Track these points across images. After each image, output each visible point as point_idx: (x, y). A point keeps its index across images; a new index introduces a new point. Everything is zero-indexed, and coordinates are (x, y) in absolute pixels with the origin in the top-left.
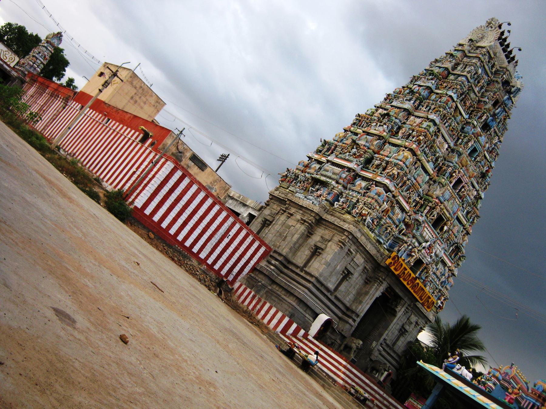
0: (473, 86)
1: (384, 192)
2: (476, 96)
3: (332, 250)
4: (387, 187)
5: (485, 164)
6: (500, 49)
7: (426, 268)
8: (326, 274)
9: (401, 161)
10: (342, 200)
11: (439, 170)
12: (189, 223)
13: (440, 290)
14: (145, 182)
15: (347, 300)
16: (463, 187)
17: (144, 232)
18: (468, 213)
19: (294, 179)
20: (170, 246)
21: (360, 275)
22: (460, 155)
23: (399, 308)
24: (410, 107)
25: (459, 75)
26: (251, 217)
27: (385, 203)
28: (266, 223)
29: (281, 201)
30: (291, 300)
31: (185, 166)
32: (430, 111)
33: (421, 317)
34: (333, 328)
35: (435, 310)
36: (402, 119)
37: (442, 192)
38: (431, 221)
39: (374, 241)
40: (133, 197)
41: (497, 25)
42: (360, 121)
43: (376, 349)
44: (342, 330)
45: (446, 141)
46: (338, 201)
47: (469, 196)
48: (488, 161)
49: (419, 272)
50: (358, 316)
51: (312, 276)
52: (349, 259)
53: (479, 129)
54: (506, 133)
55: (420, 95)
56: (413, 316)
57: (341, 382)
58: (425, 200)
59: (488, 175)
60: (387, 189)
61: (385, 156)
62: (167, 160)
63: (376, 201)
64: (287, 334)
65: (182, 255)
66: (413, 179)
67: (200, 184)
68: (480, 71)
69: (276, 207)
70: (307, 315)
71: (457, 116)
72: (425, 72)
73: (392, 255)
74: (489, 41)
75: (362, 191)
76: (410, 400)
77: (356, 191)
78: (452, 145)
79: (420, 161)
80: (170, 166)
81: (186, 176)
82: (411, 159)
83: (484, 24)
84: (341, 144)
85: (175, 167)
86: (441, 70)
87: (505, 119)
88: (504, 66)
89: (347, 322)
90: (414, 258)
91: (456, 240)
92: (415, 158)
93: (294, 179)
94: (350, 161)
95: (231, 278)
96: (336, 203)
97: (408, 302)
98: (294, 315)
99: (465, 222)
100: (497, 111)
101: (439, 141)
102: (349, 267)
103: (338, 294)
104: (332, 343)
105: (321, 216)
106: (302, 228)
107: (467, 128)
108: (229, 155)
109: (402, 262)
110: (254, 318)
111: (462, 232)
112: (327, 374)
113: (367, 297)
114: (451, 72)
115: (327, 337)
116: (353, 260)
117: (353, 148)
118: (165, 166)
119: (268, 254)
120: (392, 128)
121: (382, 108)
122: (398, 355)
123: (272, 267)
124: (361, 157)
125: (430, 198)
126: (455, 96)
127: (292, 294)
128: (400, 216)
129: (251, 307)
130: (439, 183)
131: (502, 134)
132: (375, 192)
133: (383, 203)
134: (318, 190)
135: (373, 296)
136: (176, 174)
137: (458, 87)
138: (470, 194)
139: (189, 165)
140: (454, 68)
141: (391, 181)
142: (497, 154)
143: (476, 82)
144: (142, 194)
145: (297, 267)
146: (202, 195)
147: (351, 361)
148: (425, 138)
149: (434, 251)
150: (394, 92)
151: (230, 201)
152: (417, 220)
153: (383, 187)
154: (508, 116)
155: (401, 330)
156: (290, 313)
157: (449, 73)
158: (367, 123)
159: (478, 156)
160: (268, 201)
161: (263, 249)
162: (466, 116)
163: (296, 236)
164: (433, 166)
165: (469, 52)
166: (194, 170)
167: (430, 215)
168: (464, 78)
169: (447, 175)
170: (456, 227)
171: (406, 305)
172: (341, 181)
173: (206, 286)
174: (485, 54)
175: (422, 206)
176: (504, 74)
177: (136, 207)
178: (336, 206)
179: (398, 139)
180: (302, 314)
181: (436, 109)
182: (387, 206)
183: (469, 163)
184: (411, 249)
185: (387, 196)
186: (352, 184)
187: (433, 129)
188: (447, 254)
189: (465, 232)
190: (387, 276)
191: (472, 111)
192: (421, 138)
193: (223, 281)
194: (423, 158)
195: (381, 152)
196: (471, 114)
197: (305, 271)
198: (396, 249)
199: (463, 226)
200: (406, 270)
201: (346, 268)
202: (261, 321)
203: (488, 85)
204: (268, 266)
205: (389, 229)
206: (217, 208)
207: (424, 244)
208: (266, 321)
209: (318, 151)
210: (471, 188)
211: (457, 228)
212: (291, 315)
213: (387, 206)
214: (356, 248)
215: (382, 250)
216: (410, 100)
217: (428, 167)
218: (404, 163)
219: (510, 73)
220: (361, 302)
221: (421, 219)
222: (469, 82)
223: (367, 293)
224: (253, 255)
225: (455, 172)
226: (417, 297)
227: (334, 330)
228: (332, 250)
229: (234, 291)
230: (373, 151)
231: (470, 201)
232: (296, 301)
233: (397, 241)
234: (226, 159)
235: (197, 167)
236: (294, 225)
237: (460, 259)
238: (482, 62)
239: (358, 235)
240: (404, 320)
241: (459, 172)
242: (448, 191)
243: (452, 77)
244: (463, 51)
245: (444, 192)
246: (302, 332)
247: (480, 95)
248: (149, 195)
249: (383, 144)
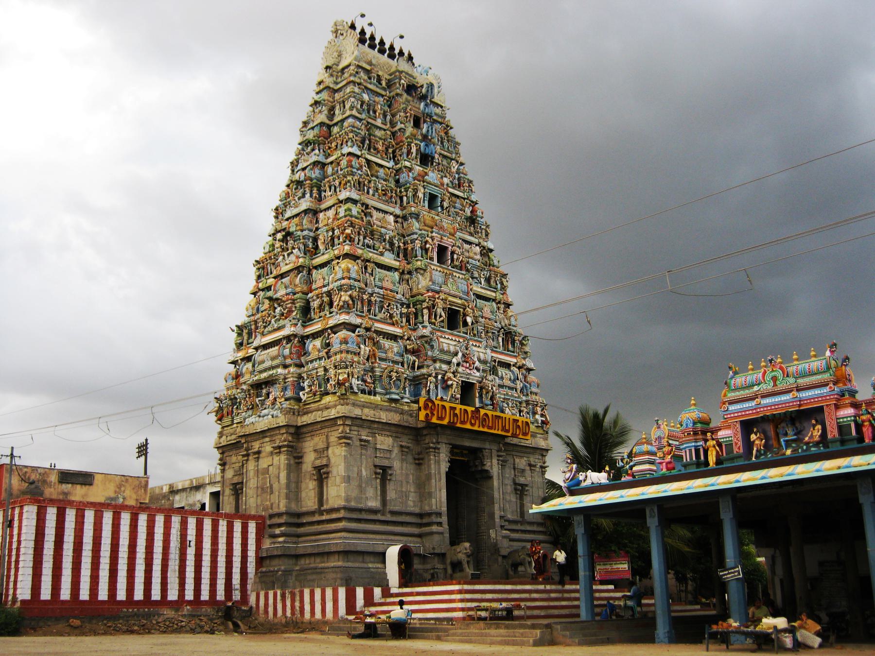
0: (370, 120)
1: (350, 333)
2: (385, 130)
3: (337, 455)
4: (350, 324)
5: (462, 205)
6: (374, 55)
7: (481, 388)
8: (354, 494)
9: (343, 278)
10: (306, 383)
11: (405, 256)
12: (120, 567)
13: (527, 402)
14: (13, 559)
15: (412, 504)
16: (453, 253)
17: (60, 626)
18: (488, 280)
19: (233, 405)
20: (115, 617)
21: (402, 460)
22: (417, 216)
23: (489, 464)
24: (308, 204)
25: (343, 121)
26: (215, 495)
27: (362, 346)
28: (238, 489)
29: (235, 446)
30: (335, 562)
31: (61, 497)
32: (338, 190)
33: (530, 453)
34: (419, 555)
35: (541, 431)
36: (310, 227)
37: (428, 279)
38: (442, 324)
39: (386, 404)
40: (11, 592)
41: (346, 27)
42: (263, 268)
43: (499, 538)
44: (434, 548)
45: (386, 212)
46: (303, 389)
47: (472, 258)
48: (464, 199)
49: (477, 400)
50: (439, 514)
51: (337, 510)
52: (370, 451)
53: (418, 168)
54: (461, 149)
55: (311, 179)
56: (517, 460)
57: (460, 614)
58: (415, 305)
59: (477, 216)
60: (351, 328)
61: (321, 287)
62: (22, 507)
63: (348, 352)
64: (358, 610)
65: (143, 617)
66: (377, 290)
67: (92, 505)
68: (366, 97)
69: (235, 459)
70: (370, 565)
71: (377, 172)
72: (300, 147)
73: (421, 403)
74: (352, 52)
75: (323, 353)
76: (598, 567)
77: (316, 360)
78: (398, 211)
79: (368, 261)
80: (30, 512)
81: (65, 509)
82: (354, 267)
83: (331, 36)
84: (259, 316)
85: (39, 508)
86: (316, 130)
87: (446, 133)
88: (393, 70)
89: (432, 533)
90: (454, 386)
91: (498, 325)
92: (359, 261)
93: (233, 405)
94: (283, 327)
95: (237, 596)
97: (494, 447)
98: (351, 579)
99: (494, 294)
100: (424, 131)
101: (377, 219)
102: (378, 462)
103: (390, 507)
104: (433, 575)
105: (295, 424)
106: (282, 460)
107: (403, 177)
108: (146, 440)
109: (441, 403)
110: (302, 623)
111: (498, 308)
112: (436, 619)
113: (433, 481)
114: (331, 123)
115: (421, 572)
116: (376, 449)
117: (275, 308)
118: (25, 516)
119: (264, 528)
120: (305, 245)
121: (280, 231)
122: (539, 524)
123: (281, 539)
124: (293, 311)
125: (420, 298)
126: (355, 150)
127: (329, 554)
128: (396, 350)
129: (289, 614)
130: (416, 270)
131: (457, 154)
132: (338, 341)
133: (359, 348)
134: (268, 395)
135: (439, 473)
136: (48, 517)
137: (351, 135)
138: (471, 255)
139: (66, 491)
140: (331, 115)
141: (348, 313)
142: (470, 182)
143: (371, 112)
144: (20, 578)
145: (312, 513)
146: (108, 518)
147: (472, 578)
148: (354, 227)
149: (476, 359)
150: (281, 200)
151: (177, 497)
152: (423, 337)
153: (345, 328)
154: (448, 126)
155: (516, 489)
156: (342, 579)
157: (329, 127)
158: (274, 264)
159: (442, 201)
160: (221, 459)
161: (252, 527)
162: (391, 164)
163: (283, 475)
164: (392, 256)
165: (336, 83)
166: (78, 493)
167: (435, 318)
168: (350, 120)
169: (419, 253)
170: (485, 309)
171: (494, 453)
172: (288, 361)
173: (207, 632)
174: (357, 73)
175: (416, 315)
176: (400, 79)
177: (23, 602)
178: (304, 398)
179: (323, 254)
180: (361, 569)
181: (343, 182)
182: (367, 349)
183: (437, 218)
184: (443, 378)
185: (358, 336)
186: (305, 354)
187: (355, 210)
188: (501, 349)
189: (502, 306)
191: (394, 152)
192: (348, 231)
193: (229, 607)
194: (371, 254)
195: (314, 287)
196: (394, 157)
197: (324, 510)
198: (423, 392)
199: (494, 300)
200: (455, 408)
201: (375, 466)
202: (313, 620)
203: (389, 106)
204: (274, 543)
205: (394, 374)
206: (160, 520)
207: (455, 360)
208: (318, 615)
209: (240, 346)
210: (466, 246)
211: (488, 308)
212: (346, 580)
213: (367, 349)
214: (368, 430)
215: (406, 408)
216: (304, 196)
217: (387, 260)
218: (350, 278)
219: (407, 73)
220: (430, 494)
221: (426, 332)
222: (360, 120)
223: (429, 477)
224: (244, 544)
225: (426, 242)
226: (500, 432)
227: (423, 558)
228: (337, 455)
229: (254, 610)
230: (304, 293)
231: (478, 264)
232: (341, 557)
233: (417, 383)
234: (147, 448)
235: (78, 487)
236: (270, 463)
237: (522, 344)
238: (359, 84)
239: (357, 412)
240: (509, 473)
241: (433, 238)
242: (436, 272)
243: (336, 130)
244: (328, 88)
245: (431, 277)
246: (377, 591)
247: (388, 125)
248: (30, 571)
249: (309, 274)
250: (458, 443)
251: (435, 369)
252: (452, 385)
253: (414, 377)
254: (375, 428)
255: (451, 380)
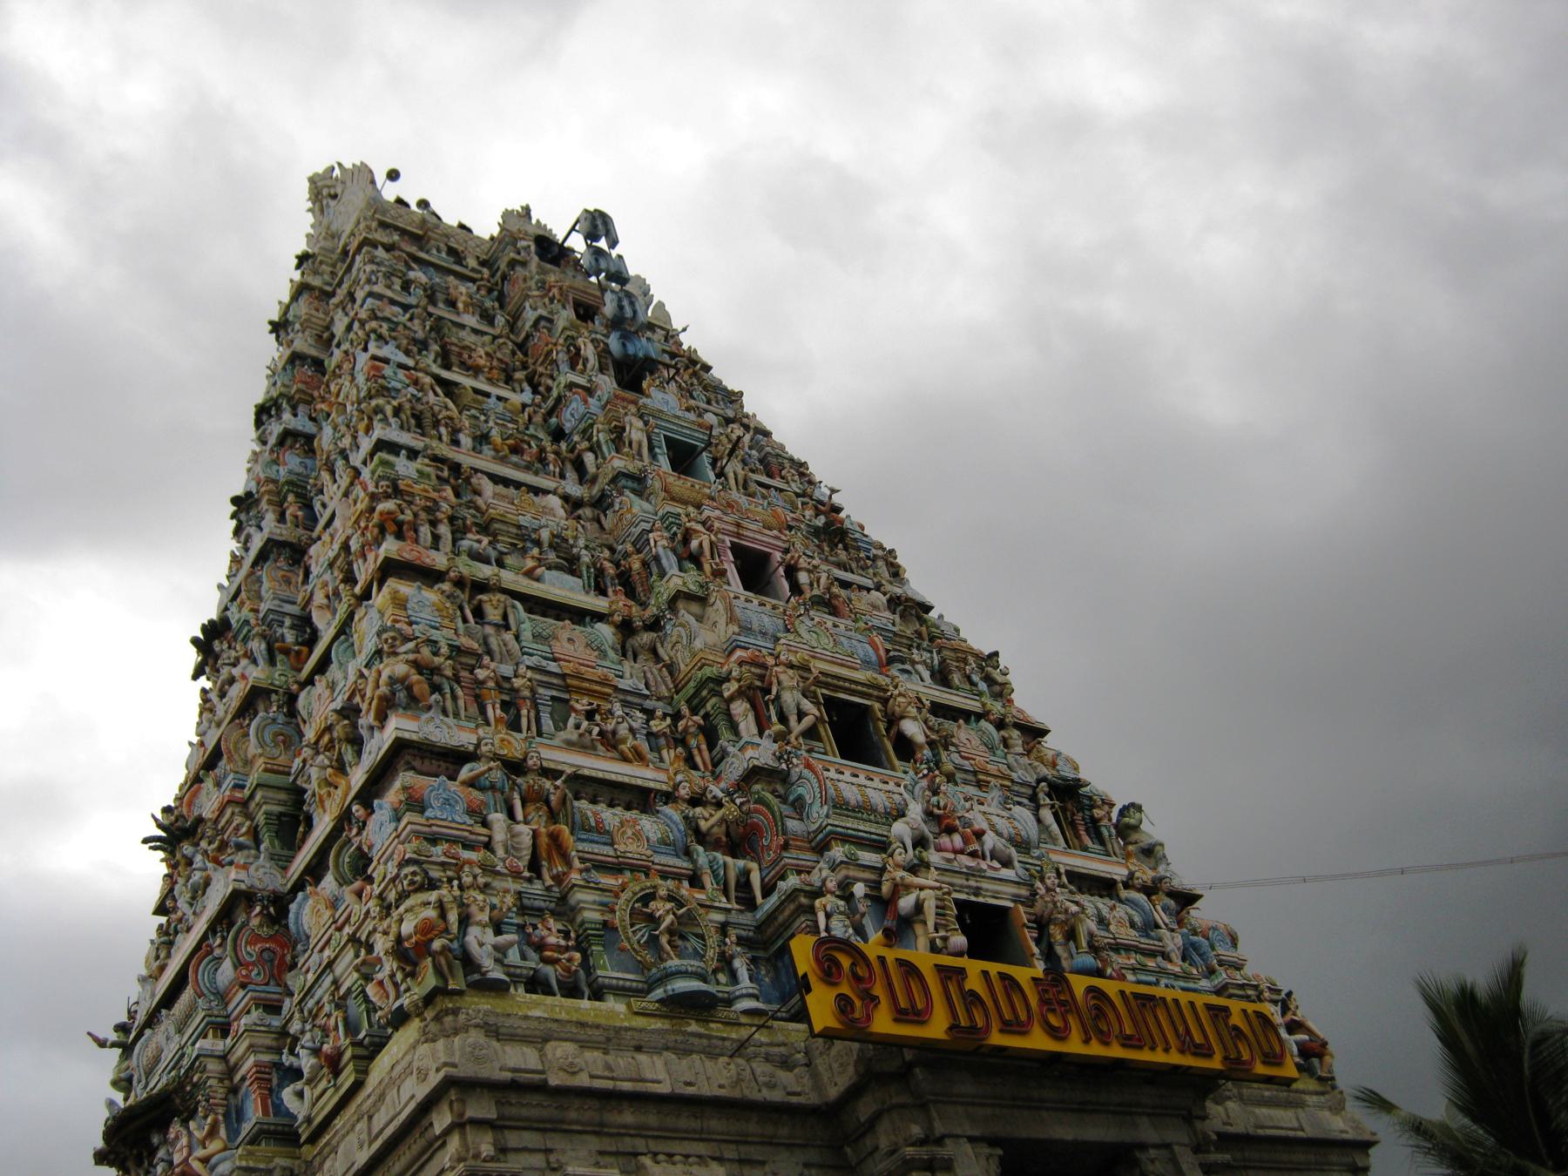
37: (722, 621)
39: (657, 1024)
78: (573, 488)
82: (425, 600)
90: (930, 907)
92: (446, 586)
96: (287, 1095)
152: (754, 774)
182: (524, 830)
184: (875, 885)
190: (924, 1107)
205: (659, 907)
214: (594, 1143)
221: (764, 753)
226: (1175, 1058)
239: (518, 1058)
250: (1024, 1133)
251: (833, 868)
252: (919, 907)
253: (759, 928)
254: (624, 1132)
255: (908, 888)
